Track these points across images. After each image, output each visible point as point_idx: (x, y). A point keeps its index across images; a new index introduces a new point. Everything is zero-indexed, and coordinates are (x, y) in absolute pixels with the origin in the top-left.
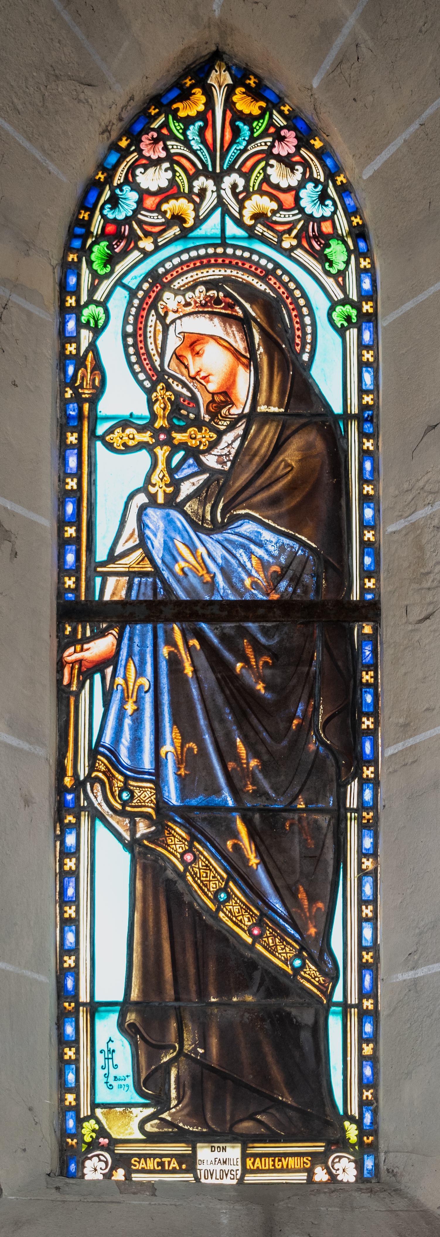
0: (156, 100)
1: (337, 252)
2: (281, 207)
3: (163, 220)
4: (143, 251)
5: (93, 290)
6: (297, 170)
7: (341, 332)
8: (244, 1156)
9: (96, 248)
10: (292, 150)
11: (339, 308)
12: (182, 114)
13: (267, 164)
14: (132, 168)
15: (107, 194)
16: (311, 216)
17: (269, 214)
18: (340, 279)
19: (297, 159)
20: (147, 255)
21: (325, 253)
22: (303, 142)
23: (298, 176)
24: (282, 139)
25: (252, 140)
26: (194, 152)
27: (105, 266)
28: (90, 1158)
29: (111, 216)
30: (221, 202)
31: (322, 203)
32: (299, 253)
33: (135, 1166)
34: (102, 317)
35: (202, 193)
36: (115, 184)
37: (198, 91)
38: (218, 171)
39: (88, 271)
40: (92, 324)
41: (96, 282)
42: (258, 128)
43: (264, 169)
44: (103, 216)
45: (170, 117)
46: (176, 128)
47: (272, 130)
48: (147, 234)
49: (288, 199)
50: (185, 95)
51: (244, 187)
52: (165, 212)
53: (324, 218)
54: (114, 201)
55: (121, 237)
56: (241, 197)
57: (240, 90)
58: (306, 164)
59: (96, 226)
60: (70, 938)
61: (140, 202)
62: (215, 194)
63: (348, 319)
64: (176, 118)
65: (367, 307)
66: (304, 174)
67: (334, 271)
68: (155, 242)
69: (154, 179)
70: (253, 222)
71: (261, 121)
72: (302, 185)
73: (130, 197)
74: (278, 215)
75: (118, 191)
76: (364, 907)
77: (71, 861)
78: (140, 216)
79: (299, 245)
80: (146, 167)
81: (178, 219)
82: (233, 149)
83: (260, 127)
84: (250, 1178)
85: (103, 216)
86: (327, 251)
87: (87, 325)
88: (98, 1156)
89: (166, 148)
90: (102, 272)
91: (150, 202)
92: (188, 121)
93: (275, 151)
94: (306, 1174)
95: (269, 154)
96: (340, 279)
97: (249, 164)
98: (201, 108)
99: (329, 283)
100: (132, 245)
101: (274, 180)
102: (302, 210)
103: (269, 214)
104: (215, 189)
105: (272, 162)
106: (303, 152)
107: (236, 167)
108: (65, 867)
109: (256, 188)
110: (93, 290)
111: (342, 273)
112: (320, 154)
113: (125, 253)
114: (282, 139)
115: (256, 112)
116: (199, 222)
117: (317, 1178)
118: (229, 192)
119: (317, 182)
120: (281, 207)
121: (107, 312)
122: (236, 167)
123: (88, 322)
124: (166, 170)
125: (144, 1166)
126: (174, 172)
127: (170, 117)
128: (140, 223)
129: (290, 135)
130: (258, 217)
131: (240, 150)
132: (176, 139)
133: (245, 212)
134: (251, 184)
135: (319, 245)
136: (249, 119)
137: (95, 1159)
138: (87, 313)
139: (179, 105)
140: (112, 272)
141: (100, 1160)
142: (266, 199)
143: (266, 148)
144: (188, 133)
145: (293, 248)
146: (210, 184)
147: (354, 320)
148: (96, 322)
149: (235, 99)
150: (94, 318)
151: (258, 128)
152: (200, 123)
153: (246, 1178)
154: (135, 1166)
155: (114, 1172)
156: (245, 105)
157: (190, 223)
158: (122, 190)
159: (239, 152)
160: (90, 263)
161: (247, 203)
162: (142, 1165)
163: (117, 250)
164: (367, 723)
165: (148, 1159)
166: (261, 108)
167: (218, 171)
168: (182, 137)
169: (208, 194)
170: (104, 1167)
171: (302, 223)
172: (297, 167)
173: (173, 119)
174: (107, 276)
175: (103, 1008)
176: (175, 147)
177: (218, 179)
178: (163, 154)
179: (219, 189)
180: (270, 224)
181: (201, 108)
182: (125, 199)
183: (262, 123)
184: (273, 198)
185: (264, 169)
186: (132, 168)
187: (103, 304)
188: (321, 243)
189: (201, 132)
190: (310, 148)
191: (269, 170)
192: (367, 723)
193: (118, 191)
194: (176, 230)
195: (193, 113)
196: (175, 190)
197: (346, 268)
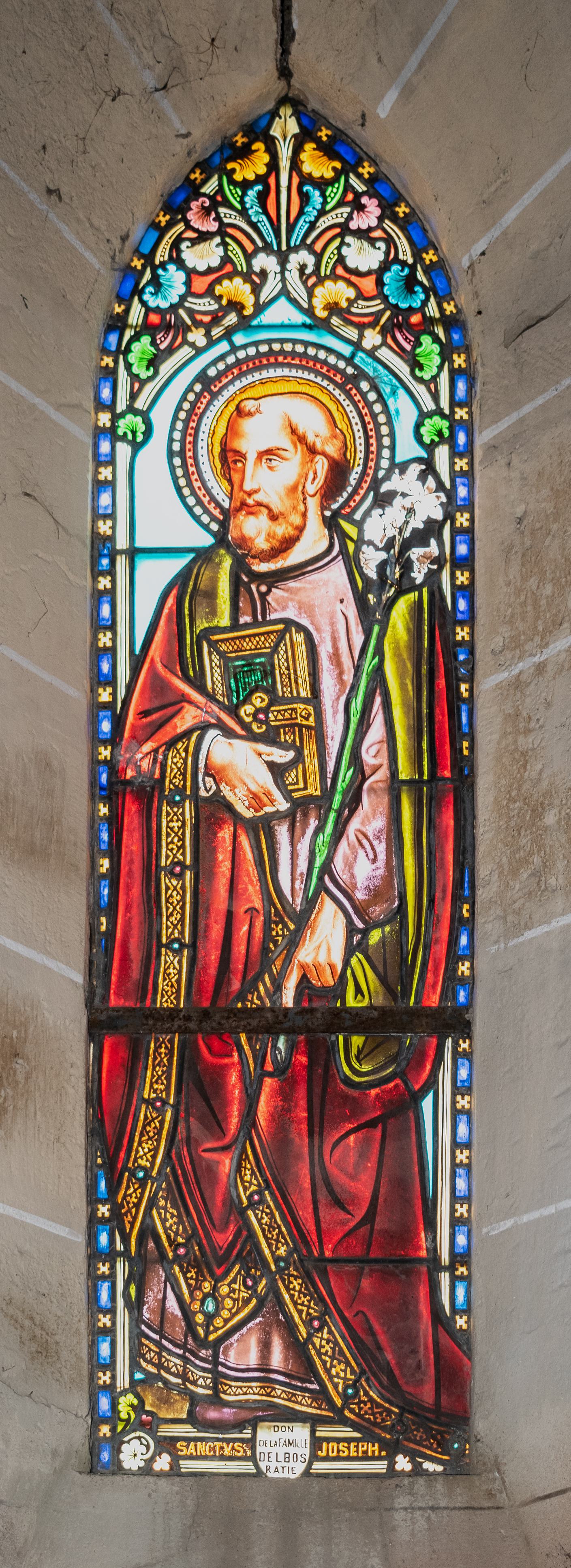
0: (206, 167)
2: (361, 295)
4: (192, 345)
5: (133, 396)
6: (379, 249)
8: (316, 1443)
10: (374, 222)
12: (238, 177)
13: (342, 243)
15: (148, 275)
16: (396, 306)
18: (432, 386)
19: (378, 234)
20: (199, 351)
22: (387, 211)
23: (381, 256)
24: (361, 208)
26: (254, 226)
28: (128, 1442)
30: (284, 292)
32: (384, 354)
33: (182, 1451)
34: (141, 428)
35: (263, 274)
36: (157, 262)
38: (284, 247)
40: (130, 437)
42: (332, 195)
44: (143, 303)
45: (225, 179)
48: (197, 324)
49: (368, 285)
50: (245, 152)
51: (314, 265)
52: (221, 297)
53: (411, 309)
55: (166, 327)
57: (309, 147)
58: (389, 241)
59: (136, 314)
60: (104, 1349)
61: (188, 283)
62: (279, 276)
63: (440, 433)
64: (231, 182)
65: (461, 413)
66: (387, 253)
67: (427, 376)
68: (208, 334)
69: (203, 256)
72: (385, 266)
73: (175, 278)
76: (458, 1151)
78: (245, 270)
79: (384, 343)
80: (194, 242)
81: (236, 306)
82: (301, 221)
83: (335, 193)
84: (319, 1467)
85: (143, 303)
88: (139, 1438)
89: (218, 218)
90: (144, 374)
92: (246, 185)
93: (353, 225)
94: (386, 1462)
96: (432, 386)
99: (421, 391)
100: (179, 340)
101: (351, 263)
102: (385, 298)
105: (348, 239)
106: (388, 224)
107: (309, 241)
109: (328, 273)
110: (133, 396)
111: (434, 378)
112: (404, 224)
113: (171, 350)
114: (361, 208)
115: (329, 174)
116: (259, 308)
117: (398, 1467)
118: (296, 274)
119: (404, 264)
120: (361, 295)
122: (309, 241)
123: (125, 434)
128: (191, 312)
129: (372, 207)
130: (333, 308)
132: (231, 207)
133: (315, 302)
135: (409, 343)
136: (322, 184)
140: (156, 372)
142: (341, 284)
144: (247, 199)
145: (375, 348)
147: (446, 433)
148: (134, 433)
151: (332, 195)
152: (259, 187)
153: (313, 1467)
154: (182, 1451)
155: (158, 1458)
156: (315, 164)
157: (248, 312)
159: (307, 225)
160: (128, 366)
161: (318, 291)
162: (191, 1450)
166: (334, 169)
167: (284, 247)
168: (239, 206)
169: (271, 276)
170: (145, 1451)
174: (150, 379)
177: (283, 262)
178: (214, 227)
183: (338, 188)
184: (350, 283)
185: (339, 248)
186: (179, 240)
187: (145, 415)
189: (262, 198)
190: (395, 218)
191: (345, 250)
193: (160, 272)
194: (232, 319)
195: (251, 177)
196: (228, 268)
197: (438, 375)
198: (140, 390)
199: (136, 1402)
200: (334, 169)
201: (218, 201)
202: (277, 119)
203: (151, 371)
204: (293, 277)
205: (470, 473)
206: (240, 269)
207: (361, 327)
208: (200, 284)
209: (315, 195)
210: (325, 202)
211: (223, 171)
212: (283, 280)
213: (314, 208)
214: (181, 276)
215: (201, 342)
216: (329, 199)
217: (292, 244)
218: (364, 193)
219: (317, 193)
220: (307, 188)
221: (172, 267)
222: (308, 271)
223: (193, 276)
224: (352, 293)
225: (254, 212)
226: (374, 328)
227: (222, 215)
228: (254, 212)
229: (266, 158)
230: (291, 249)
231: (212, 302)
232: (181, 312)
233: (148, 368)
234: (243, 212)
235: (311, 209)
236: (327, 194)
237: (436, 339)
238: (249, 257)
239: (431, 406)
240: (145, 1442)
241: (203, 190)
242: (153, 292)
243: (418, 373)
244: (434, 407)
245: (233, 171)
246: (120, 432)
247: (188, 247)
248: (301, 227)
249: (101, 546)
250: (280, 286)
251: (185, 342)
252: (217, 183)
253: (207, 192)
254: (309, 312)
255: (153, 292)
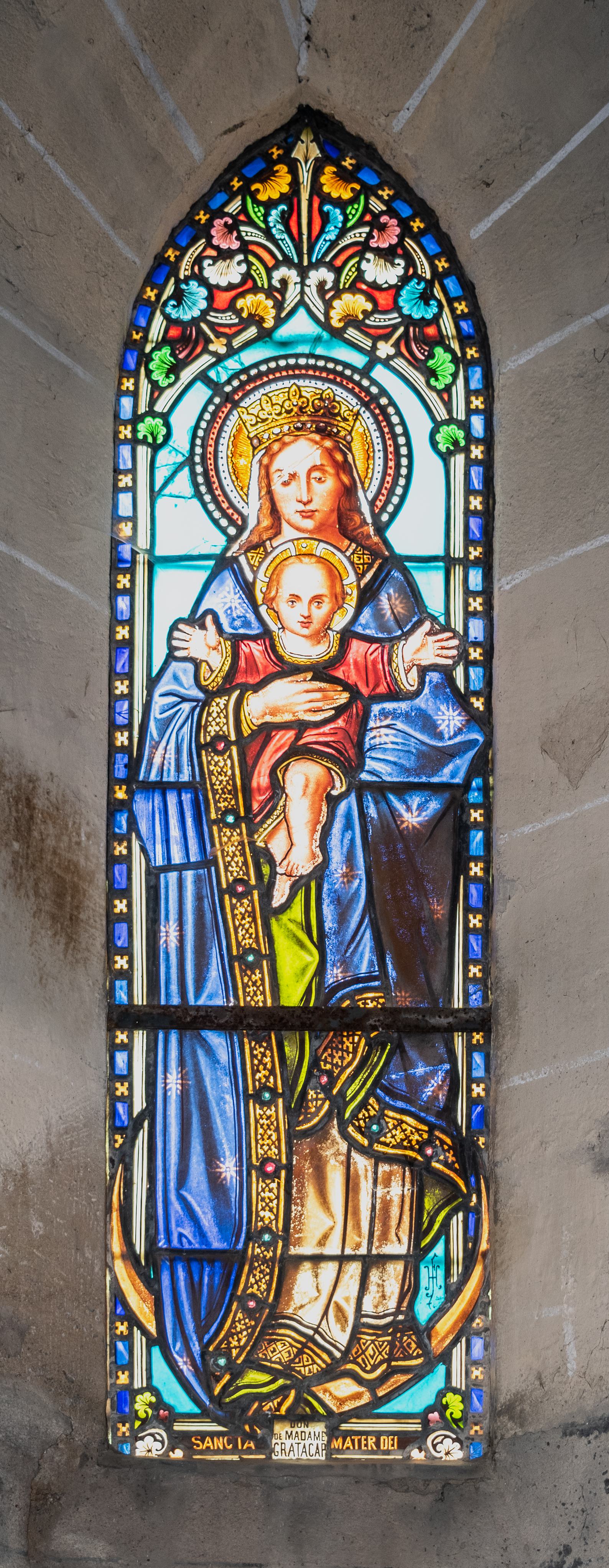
1: (442, 360)
2: (375, 311)
3: (237, 321)
5: (152, 402)
6: (399, 264)
7: (445, 457)
9: (156, 355)
11: (444, 429)
12: (262, 197)
14: (198, 261)
15: (170, 289)
17: (361, 317)
21: (428, 364)
23: (400, 271)
24: (383, 228)
25: (343, 232)
27: (167, 376)
28: (142, 1439)
29: (174, 315)
30: (302, 303)
31: (427, 304)
35: (284, 282)
37: (282, 169)
38: (305, 263)
39: (146, 381)
40: (150, 440)
41: (156, 394)
43: (359, 263)
44: (167, 317)
45: (249, 201)
46: (256, 213)
47: (368, 218)
48: (218, 335)
49: (383, 299)
50: (266, 175)
51: (333, 282)
54: (179, 296)
55: (186, 340)
56: (328, 296)
57: (329, 169)
58: (410, 262)
61: (210, 298)
62: (299, 286)
64: (256, 202)
66: (406, 269)
70: (341, 325)
71: (356, 206)
72: (405, 280)
74: (372, 318)
75: (183, 286)
77: (126, 429)
78: (208, 318)
79: (399, 354)
80: (215, 260)
81: (255, 320)
82: (321, 241)
85: (167, 317)
86: (430, 363)
87: (144, 441)
89: (239, 238)
90: (163, 383)
91: (223, 298)
92: (270, 205)
93: (373, 244)
95: (364, 247)
97: (342, 258)
98: (285, 189)
99: (432, 398)
100: (199, 350)
103: (361, 317)
104: (298, 280)
105: (369, 255)
107: (328, 259)
108: (122, 576)
109: (347, 286)
110: (152, 402)
111: (448, 389)
115: (347, 195)
116: (280, 321)
118: (314, 289)
119: (421, 279)
121: (167, 425)
123: (145, 437)
124: (239, 263)
125: (210, 1444)
126: (250, 264)
127: (249, 201)
128: (212, 326)
130: (350, 321)
131: (330, 240)
132: (251, 223)
133: (332, 313)
134: (342, 280)
135: (423, 354)
136: (341, 204)
137: (149, 1439)
138: (143, 429)
139: (257, 186)
140: (177, 379)
141: (156, 1440)
143: (362, 240)
144: (270, 219)
145: (389, 358)
146: (293, 275)
147: (462, 443)
149: (323, 179)
150: (152, 434)
154: (198, 1445)
157: (269, 324)
158: (187, 284)
159: (328, 243)
160: (149, 373)
161: (336, 303)
163: (181, 356)
164: (476, 921)
165: (215, 1439)
167: (305, 263)
168: (263, 226)
169: (291, 287)
171: (401, 329)
172: (397, 261)
173: (253, 203)
174: (170, 385)
175: (152, 1037)
176: (249, 234)
177: (303, 274)
179: (303, 283)
180: (359, 325)
181: (285, 189)
182: (190, 293)
184: (370, 298)
185: (359, 263)
186: (198, 261)
187: (165, 417)
188: (425, 351)
189: (285, 219)
191: (364, 265)
192: (476, 921)
194: (252, 331)
195: (275, 196)
196: (249, 284)
197: (454, 382)
198: (159, 397)
199: (154, 1399)
200: (353, 190)
201: (243, 218)
202: (300, 142)
203: (173, 377)
204: (312, 292)
205: (111, 783)
206: (260, 285)
207: (376, 339)
208: (223, 298)
209: (336, 214)
210: (346, 220)
211: (245, 191)
212: (302, 293)
213: (336, 227)
214: (203, 292)
215: (223, 350)
216: (350, 217)
217: (314, 260)
218: (382, 213)
219: (338, 211)
220: (327, 208)
221: (193, 284)
222: (329, 285)
223: (215, 290)
224: (369, 307)
225: (278, 231)
226: (386, 342)
227: (244, 234)
228: (278, 231)
229: (289, 178)
230: (313, 266)
231: (233, 317)
232: (204, 326)
233: (167, 376)
234: (267, 233)
235: (333, 228)
236: (348, 212)
237: (448, 349)
238: (269, 271)
239: (441, 413)
240: (439, 1439)
241: (226, 210)
242: (175, 303)
243: (433, 381)
244: (447, 417)
245: (258, 191)
246: (140, 436)
247: (209, 265)
248: (321, 246)
249: (119, 565)
250: (298, 297)
251: (205, 350)
252: (240, 203)
253: (230, 211)
254: (326, 325)
255: (175, 303)
